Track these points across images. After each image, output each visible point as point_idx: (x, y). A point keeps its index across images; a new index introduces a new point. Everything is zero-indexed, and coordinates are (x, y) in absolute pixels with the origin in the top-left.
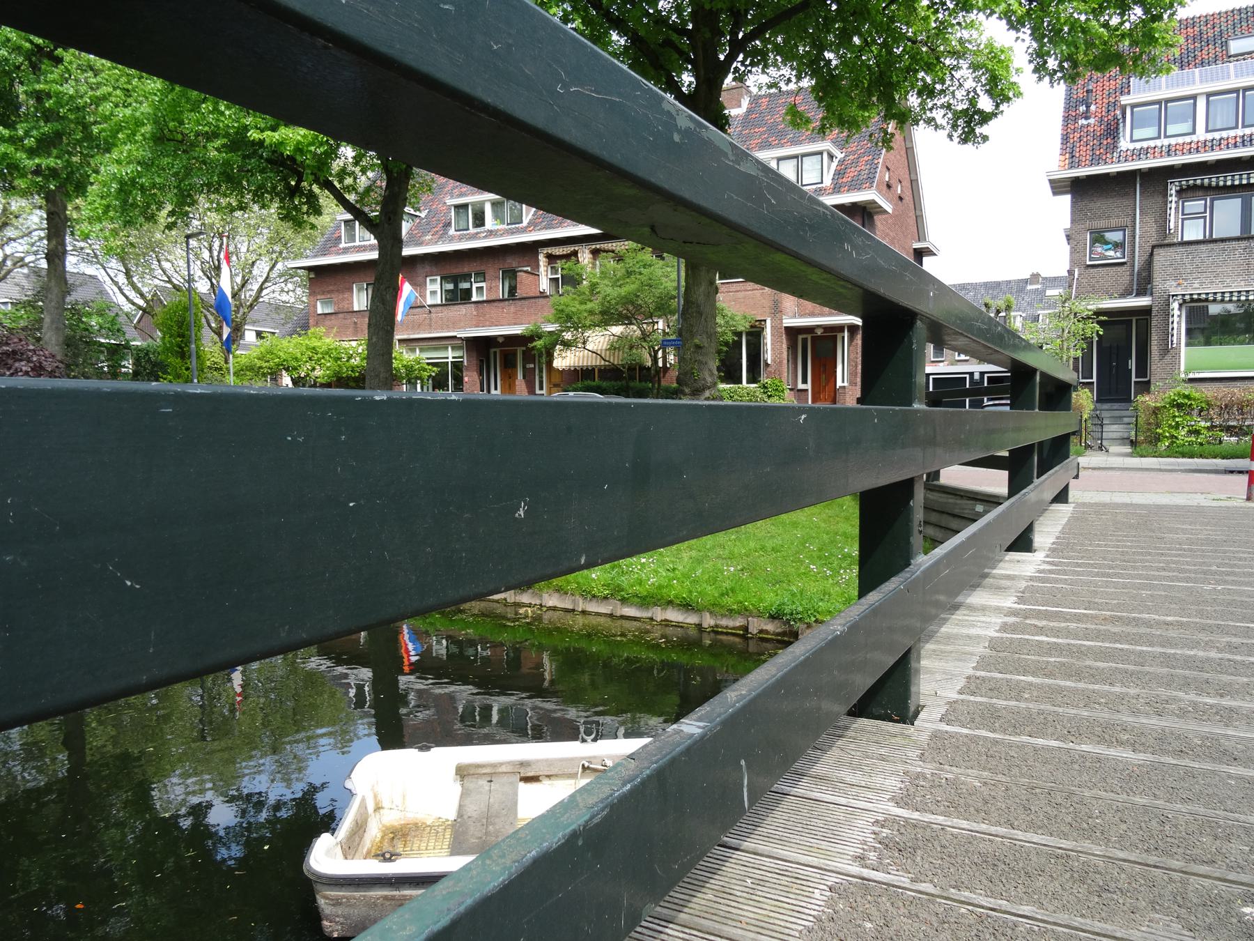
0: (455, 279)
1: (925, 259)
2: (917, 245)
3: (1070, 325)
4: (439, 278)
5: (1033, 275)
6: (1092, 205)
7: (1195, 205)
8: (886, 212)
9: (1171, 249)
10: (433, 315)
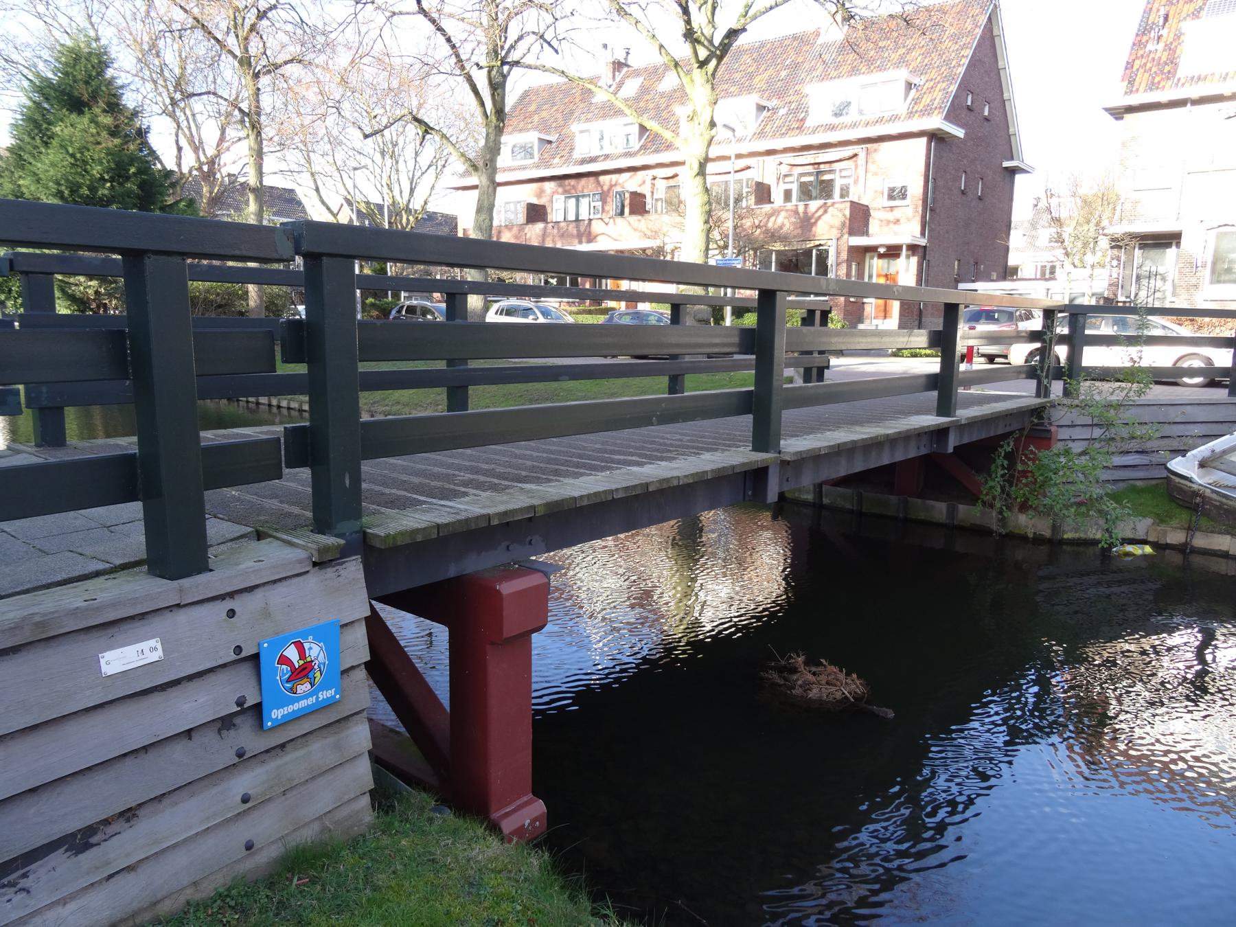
2: (1006, 164)
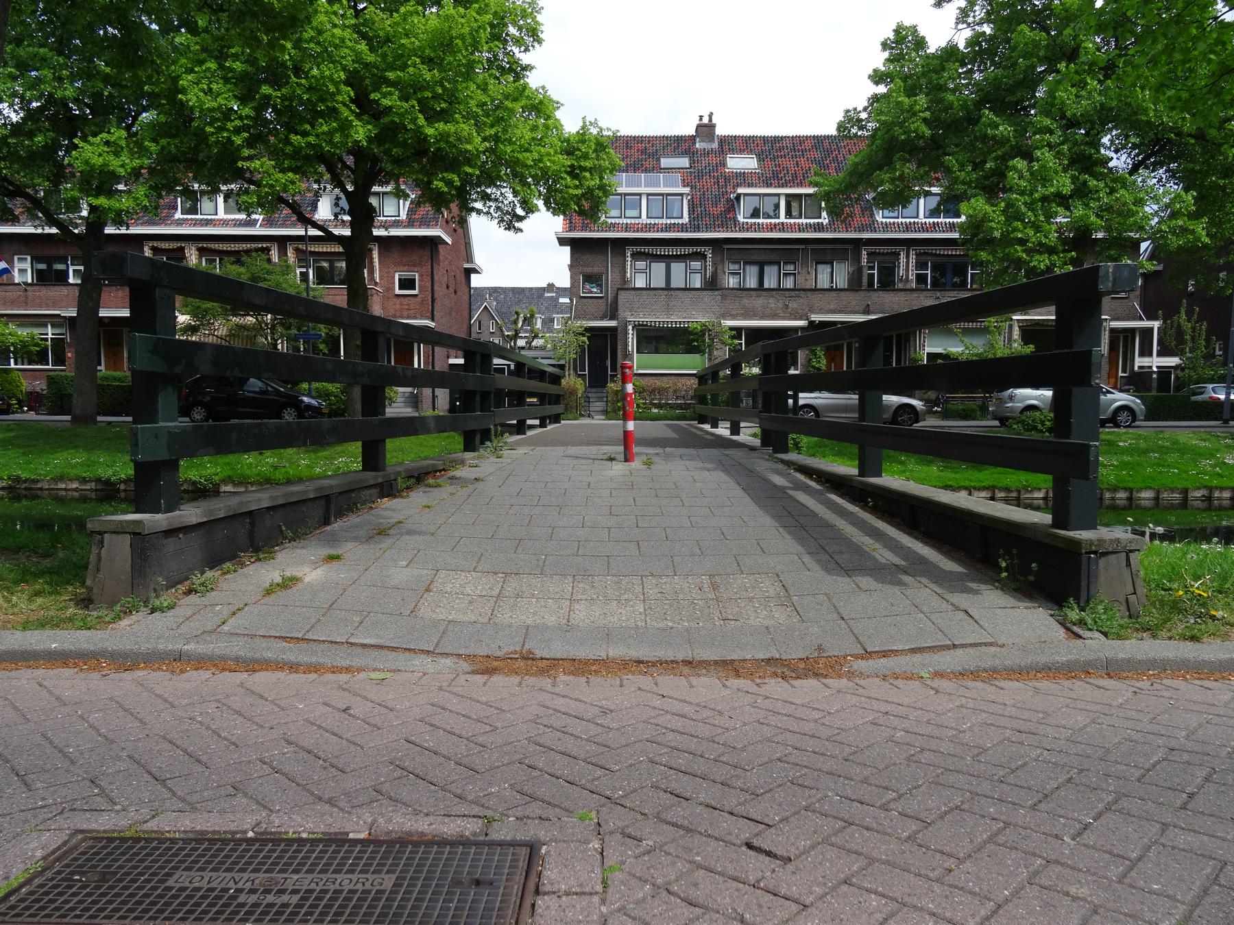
0: (49, 261)
1: (473, 276)
2: (467, 266)
3: (571, 337)
4: (29, 258)
5: (549, 285)
6: (583, 257)
7: (641, 264)
8: (447, 243)
9: (627, 292)
10: (30, 294)
